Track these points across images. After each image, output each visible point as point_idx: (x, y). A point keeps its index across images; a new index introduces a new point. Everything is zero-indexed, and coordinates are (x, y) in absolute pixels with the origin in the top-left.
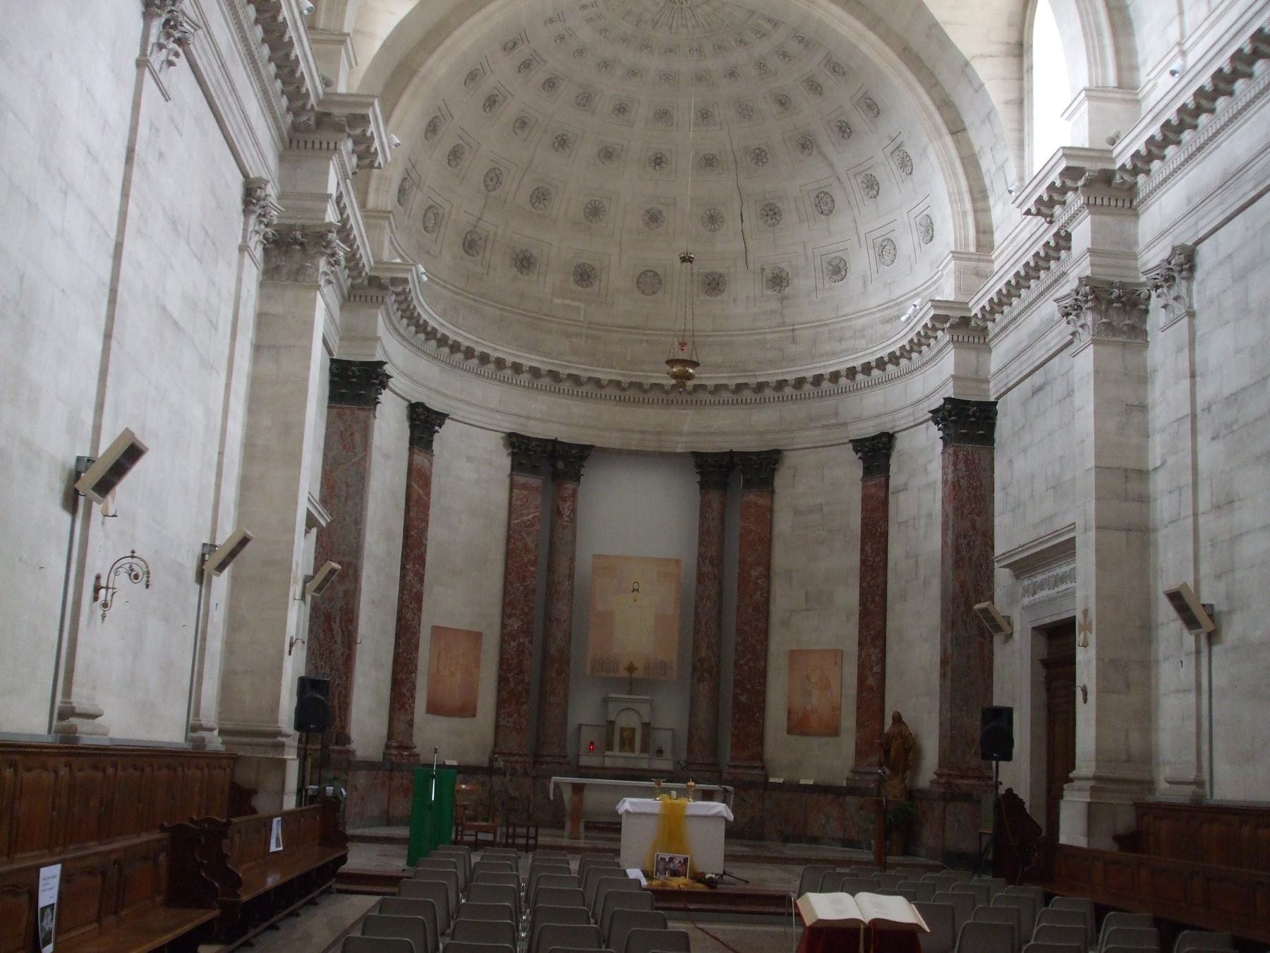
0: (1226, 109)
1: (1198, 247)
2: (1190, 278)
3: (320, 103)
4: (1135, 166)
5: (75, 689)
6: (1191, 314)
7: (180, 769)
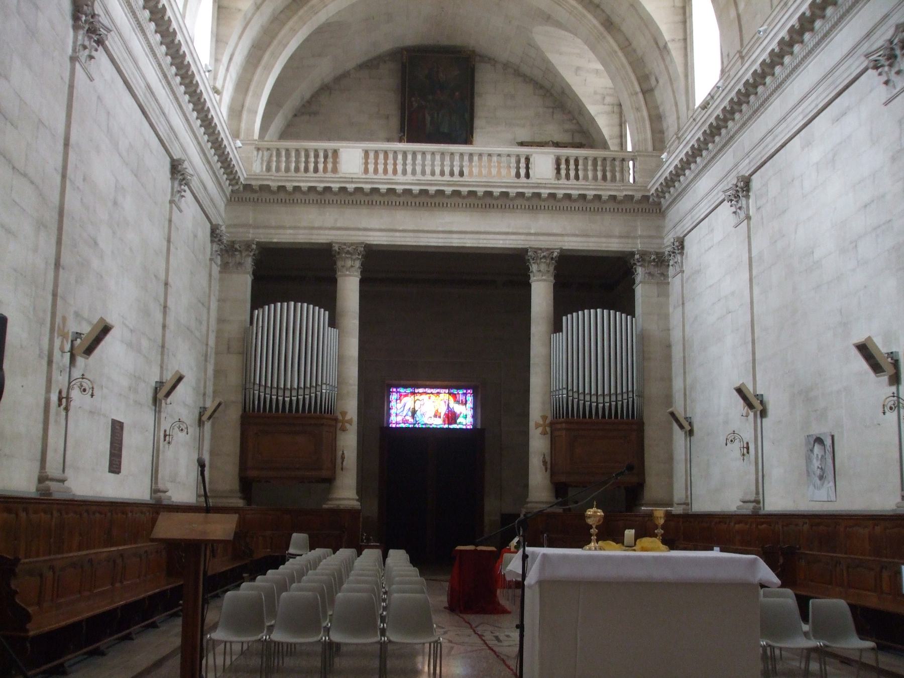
0: (707, 155)
1: (753, 177)
2: (747, 197)
3: (246, 179)
4: (772, 61)
5: (48, 464)
6: (748, 218)
7: (109, 514)
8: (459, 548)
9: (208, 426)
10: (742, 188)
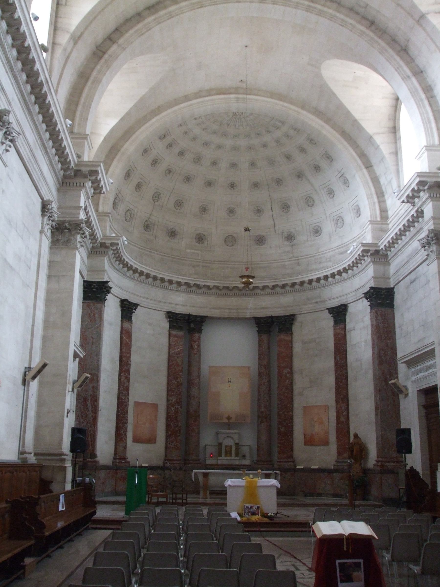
3: (76, 165)
8: (377, 538)
9: (34, 385)
10: (432, 238)
